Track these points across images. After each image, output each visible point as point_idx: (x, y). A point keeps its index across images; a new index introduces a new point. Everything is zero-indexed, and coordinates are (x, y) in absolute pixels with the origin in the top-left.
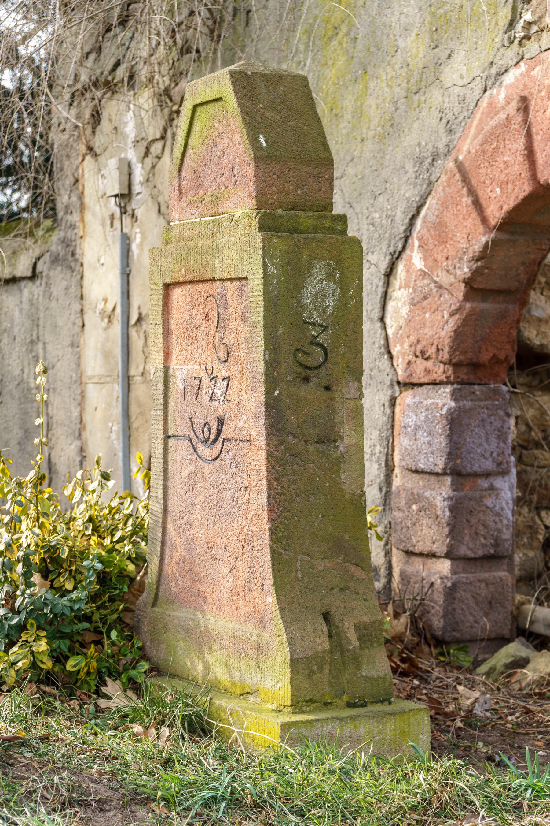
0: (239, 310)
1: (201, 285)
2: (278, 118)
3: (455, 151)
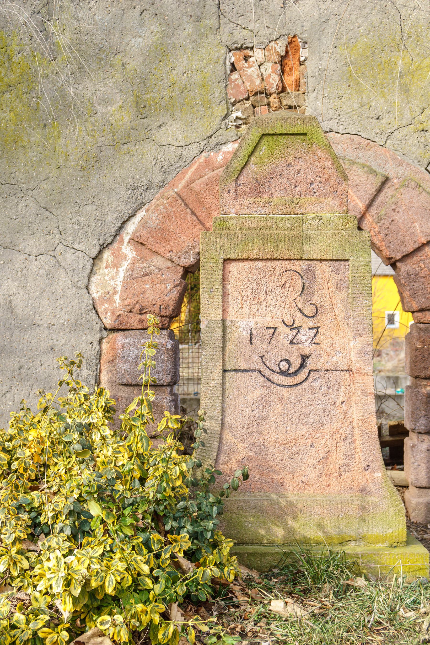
1: (270, 262)
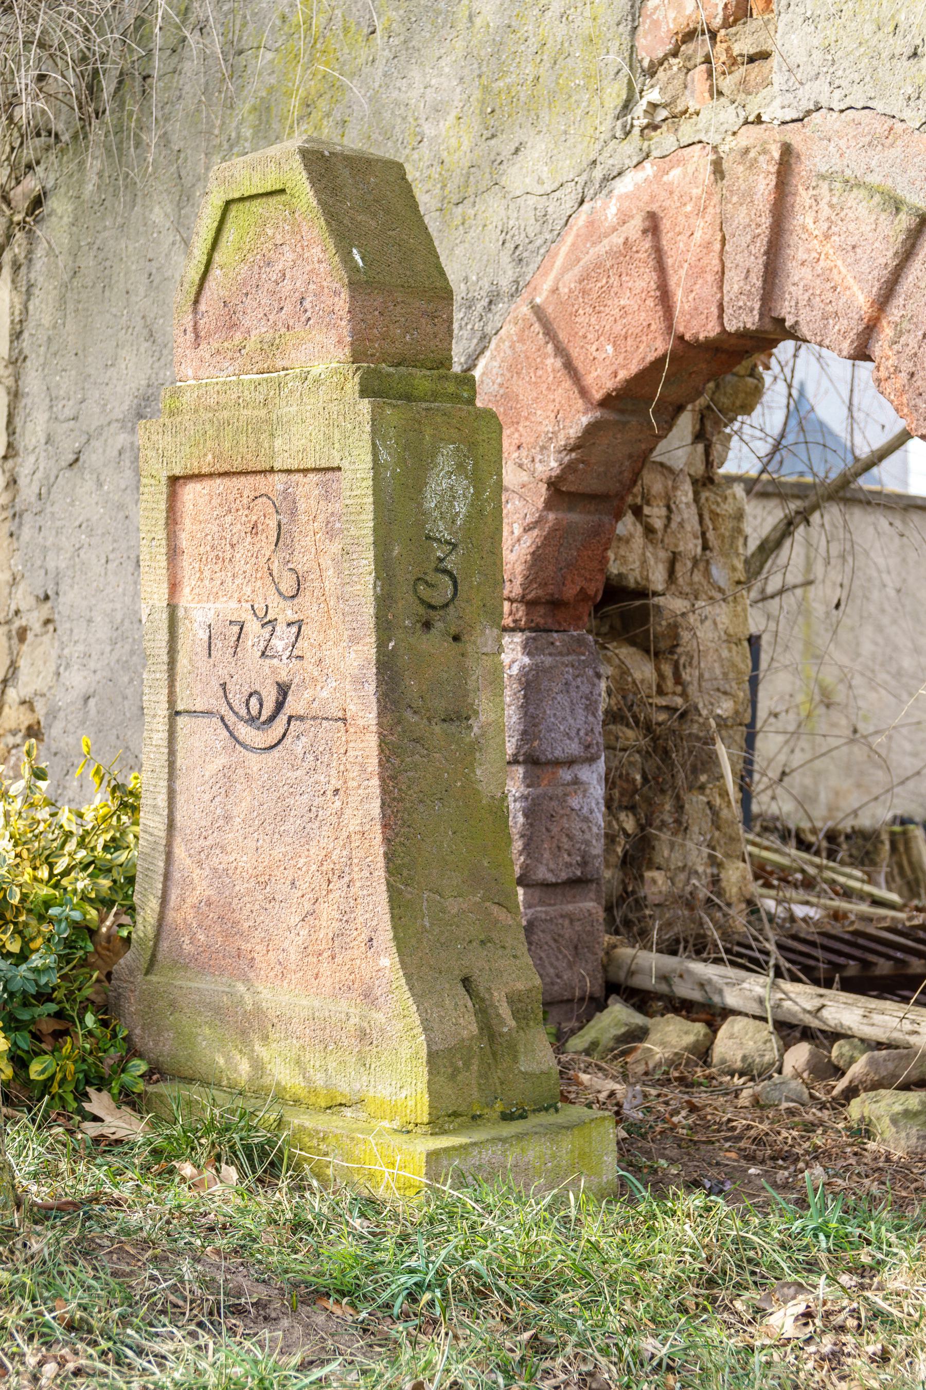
0: (321, 518)
2: (373, 223)
3: (529, 289)
